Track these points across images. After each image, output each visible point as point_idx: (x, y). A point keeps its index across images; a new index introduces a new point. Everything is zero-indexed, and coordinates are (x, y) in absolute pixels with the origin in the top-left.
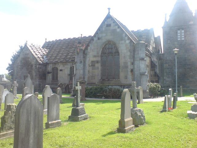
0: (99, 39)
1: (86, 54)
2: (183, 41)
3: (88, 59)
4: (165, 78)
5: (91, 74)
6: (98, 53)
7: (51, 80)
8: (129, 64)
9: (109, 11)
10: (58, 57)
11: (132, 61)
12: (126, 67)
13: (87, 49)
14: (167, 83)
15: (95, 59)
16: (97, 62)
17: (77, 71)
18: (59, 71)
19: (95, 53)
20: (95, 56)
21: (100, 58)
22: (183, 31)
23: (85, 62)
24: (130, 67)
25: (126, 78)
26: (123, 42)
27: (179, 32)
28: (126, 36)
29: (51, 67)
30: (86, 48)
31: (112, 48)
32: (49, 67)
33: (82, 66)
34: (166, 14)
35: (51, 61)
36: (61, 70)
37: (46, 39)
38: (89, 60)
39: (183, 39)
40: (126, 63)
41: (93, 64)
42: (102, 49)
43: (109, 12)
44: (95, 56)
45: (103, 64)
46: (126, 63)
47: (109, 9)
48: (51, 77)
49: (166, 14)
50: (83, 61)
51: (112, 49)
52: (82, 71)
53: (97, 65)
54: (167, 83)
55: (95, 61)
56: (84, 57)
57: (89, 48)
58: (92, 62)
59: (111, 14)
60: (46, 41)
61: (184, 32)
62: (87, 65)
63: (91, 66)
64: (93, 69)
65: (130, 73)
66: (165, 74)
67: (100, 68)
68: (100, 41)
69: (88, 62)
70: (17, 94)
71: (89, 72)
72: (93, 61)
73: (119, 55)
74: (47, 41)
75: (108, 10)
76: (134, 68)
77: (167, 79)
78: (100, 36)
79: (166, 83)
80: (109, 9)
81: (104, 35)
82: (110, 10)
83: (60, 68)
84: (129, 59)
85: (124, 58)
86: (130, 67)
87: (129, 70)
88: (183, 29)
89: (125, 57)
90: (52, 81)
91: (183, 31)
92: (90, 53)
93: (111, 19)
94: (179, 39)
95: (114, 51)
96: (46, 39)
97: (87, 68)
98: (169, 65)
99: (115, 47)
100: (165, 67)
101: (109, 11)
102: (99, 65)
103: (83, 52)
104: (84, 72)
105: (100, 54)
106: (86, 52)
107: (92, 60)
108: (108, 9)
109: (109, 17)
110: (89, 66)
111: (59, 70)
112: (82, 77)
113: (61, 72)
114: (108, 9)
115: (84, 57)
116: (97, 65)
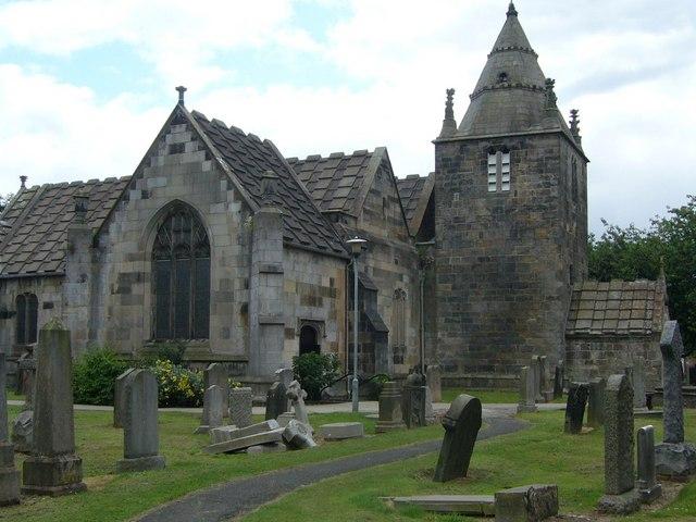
0: (145, 195)
1: (103, 250)
2: (506, 194)
3: (109, 267)
4: (439, 335)
5: (117, 323)
6: (141, 246)
7: (12, 342)
8: (237, 285)
9: (181, 96)
10: (41, 256)
11: (247, 275)
12: (229, 297)
13: (107, 232)
14: (448, 353)
15: (130, 268)
16: (139, 278)
17: (69, 310)
18: (40, 311)
19: (131, 246)
20: (131, 258)
21: (148, 263)
22: (506, 159)
23: (97, 276)
24: (239, 298)
25: (226, 333)
26: (221, 207)
27: (492, 160)
28: (229, 188)
29: (12, 292)
30: (104, 229)
31: (190, 231)
32: (8, 291)
33: (87, 292)
34: (450, 93)
35: (15, 268)
36: (48, 306)
37: (23, 179)
38: (113, 270)
39: (506, 188)
40: (226, 282)
41: (125, 284)
42: (154, 234)
43: (181, 102)
44: (131, 258)
45: (160, 287)
46: (226, 282)
47: (181, 90)
48: (12, 333)
49: (450, 93)
50: (89, 276)
51: (187, 231)
52: (84, 313)
53: (136, 289)
54: (448, 353)
55: (129, 274)
56: (96, 261)
57: (113, 227)
58: (123, 276)
59: (189, 107)
60: (23, 186)
61: (508, 161)
62: (105, 290)
63: (118, 292)
64: (123, 304)
65: (237, 318)
66: (441, 320)
67: (148, 299)
68: (148, 202)
69: (108, 279)
70: (160, 407)
71: (110, 311)
72: (124, 275)
73: (209, 254)
74: (29, 185)
75: (177, 93)
76: (250, 301)
77: (449, 341)
78: (150, 184)
79: (442, 355)
80: (181, 90)
81: (162, 181)
82: (185, 93)
83: (43, 298)
84: (236, 269)
85: (224, 265)
86: (239, 297)
87: (237, 308)
88: (505, 151)
89: (223, 262)
90: (15, 348)
91: (506, 159)
92: (116, 247)
93: (184, 126)
94: (492, 189)
95: (193, 238)
96: (23, 179)
97: (107, 298)
98: (454, 288)
99: (196, 226)
100: (439, 294)
101: (181, 96)
102: (144, 291)
103: (89, 241)
104: (94, 313)
105: (149, 249)
106: (103, 241)
107: (122, 272)
108: (178, 89)
109: (178, 117)
110: (113, 293)
111: (41, 305)
112: (88, 331)
113: (48, 311)
114: (178, 89)
115: (95, 261)
116: (136, 289)
